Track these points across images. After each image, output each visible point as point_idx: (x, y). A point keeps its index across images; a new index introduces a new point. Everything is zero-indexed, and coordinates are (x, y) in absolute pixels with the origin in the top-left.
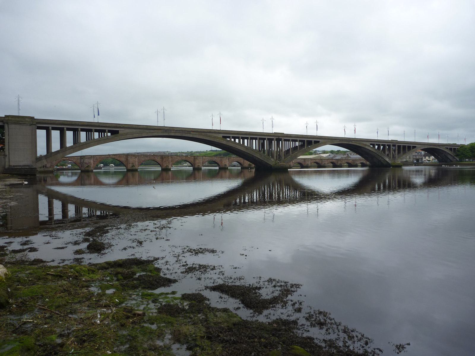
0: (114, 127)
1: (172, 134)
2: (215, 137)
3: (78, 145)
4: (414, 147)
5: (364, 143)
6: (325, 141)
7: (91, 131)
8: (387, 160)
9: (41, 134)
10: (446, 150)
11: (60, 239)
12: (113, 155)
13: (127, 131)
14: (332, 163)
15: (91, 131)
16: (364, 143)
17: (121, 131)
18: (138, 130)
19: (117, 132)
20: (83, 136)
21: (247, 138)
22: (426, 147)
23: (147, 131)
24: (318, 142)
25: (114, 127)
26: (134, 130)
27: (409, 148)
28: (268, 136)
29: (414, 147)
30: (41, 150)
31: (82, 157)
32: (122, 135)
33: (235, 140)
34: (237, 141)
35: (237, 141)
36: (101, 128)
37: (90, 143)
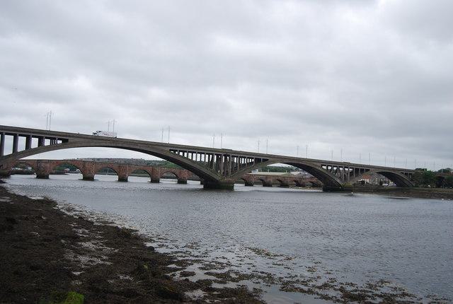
0: (64, 136)
1: (120, 145)
2: (162, 150)
3: (29, 151)
4: (367, 170)
5: (315, 163)
6: (275, 159)
7: (55, 139)
8: (338, 181)
9: (9, 140)
10: (402, 176)
11: (253, 246)
12: (70, 160)
13: (77, 140)
14: (295, 181)
15: (55, 139)
16: (315, 163)
17: (71, 140)
18: (87, 140)
19: (67, 141)
20: (47, 142)
21: (237, 157)
22: (380, 171)
23: (95, 141)
24: (369, 170)
25: (64, 136)
26: (83, 140)
27: (362, 170)
28: (6, 130)
29: (367, 170)
30: (8, 151)
31: (39, 161)
32: (71, 143)
33: (41, 143)
34: (181, 154)
35: (186, 155)
36: (53, 136)
37: (41, 148)
